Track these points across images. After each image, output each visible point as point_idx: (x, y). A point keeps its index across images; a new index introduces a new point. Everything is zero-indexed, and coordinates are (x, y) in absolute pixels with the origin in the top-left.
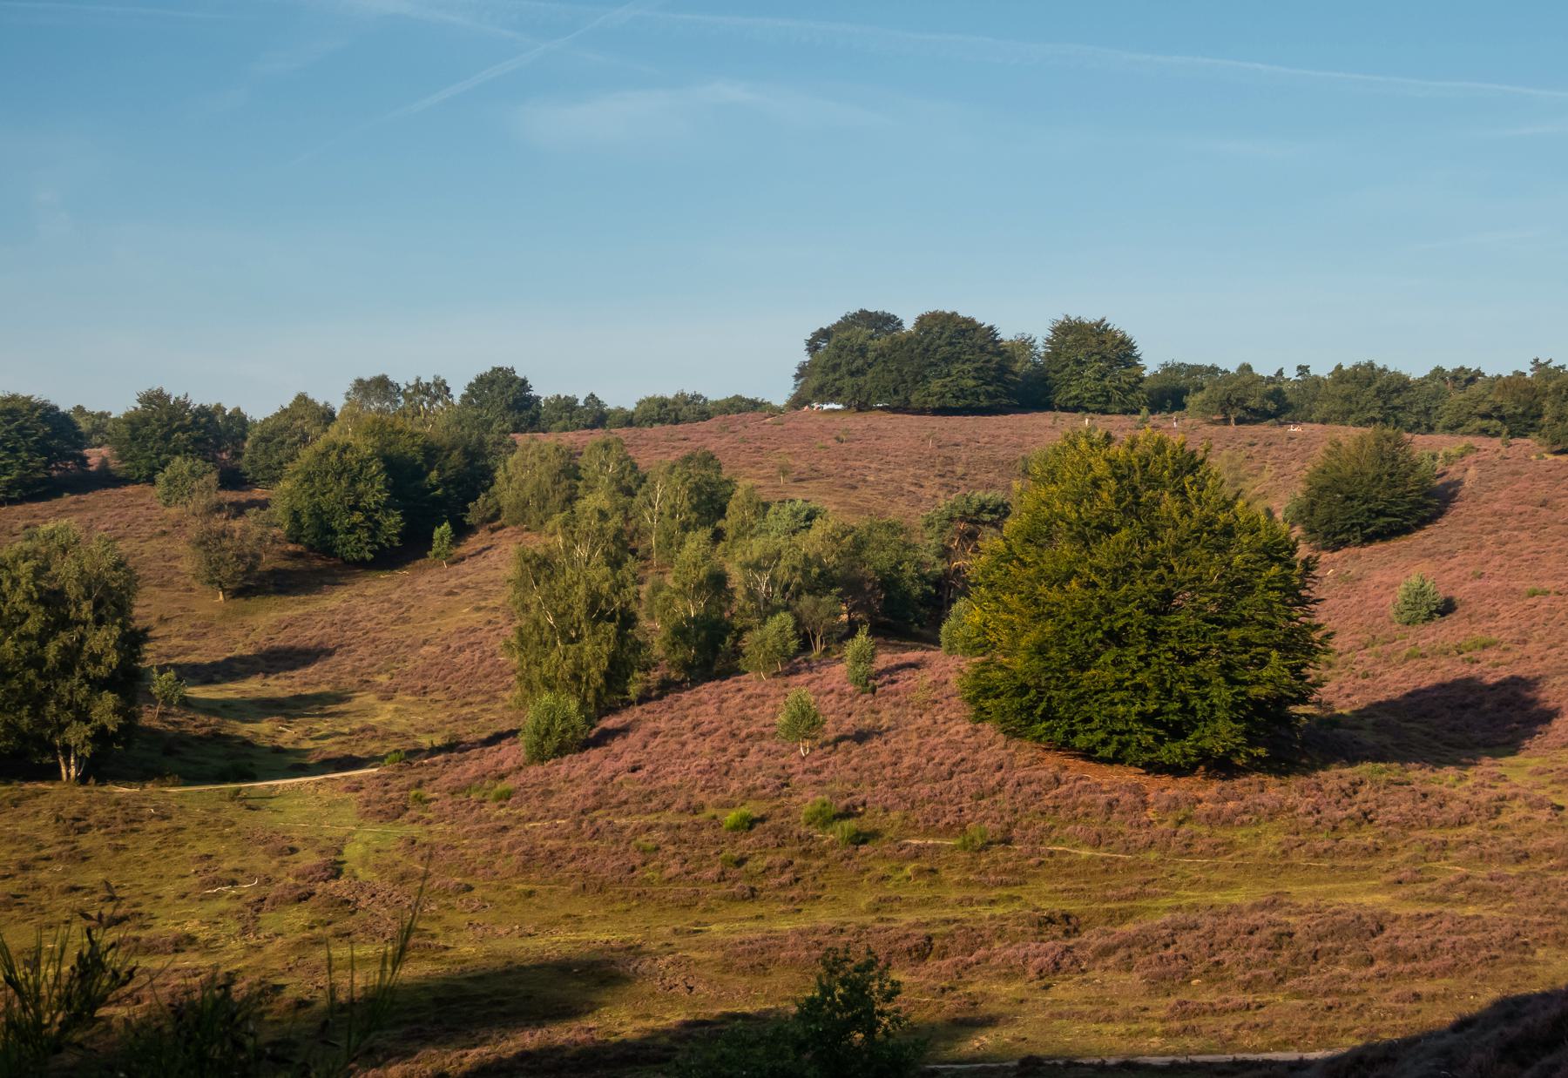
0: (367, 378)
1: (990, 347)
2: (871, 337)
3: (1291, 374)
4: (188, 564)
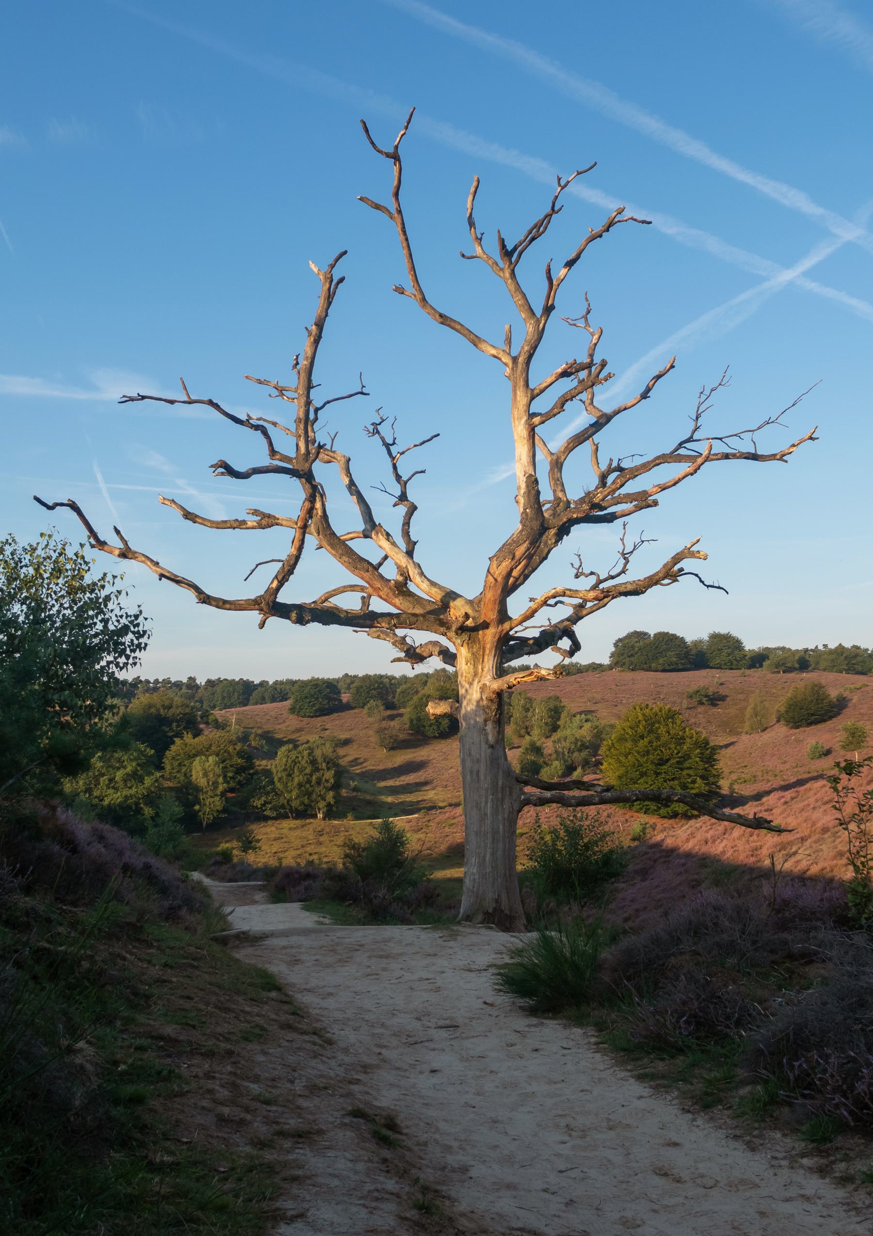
0: (438, 669)
1: (682, 645)
2: (636, 642)
3: (821, 647)
4: (374, 739)
